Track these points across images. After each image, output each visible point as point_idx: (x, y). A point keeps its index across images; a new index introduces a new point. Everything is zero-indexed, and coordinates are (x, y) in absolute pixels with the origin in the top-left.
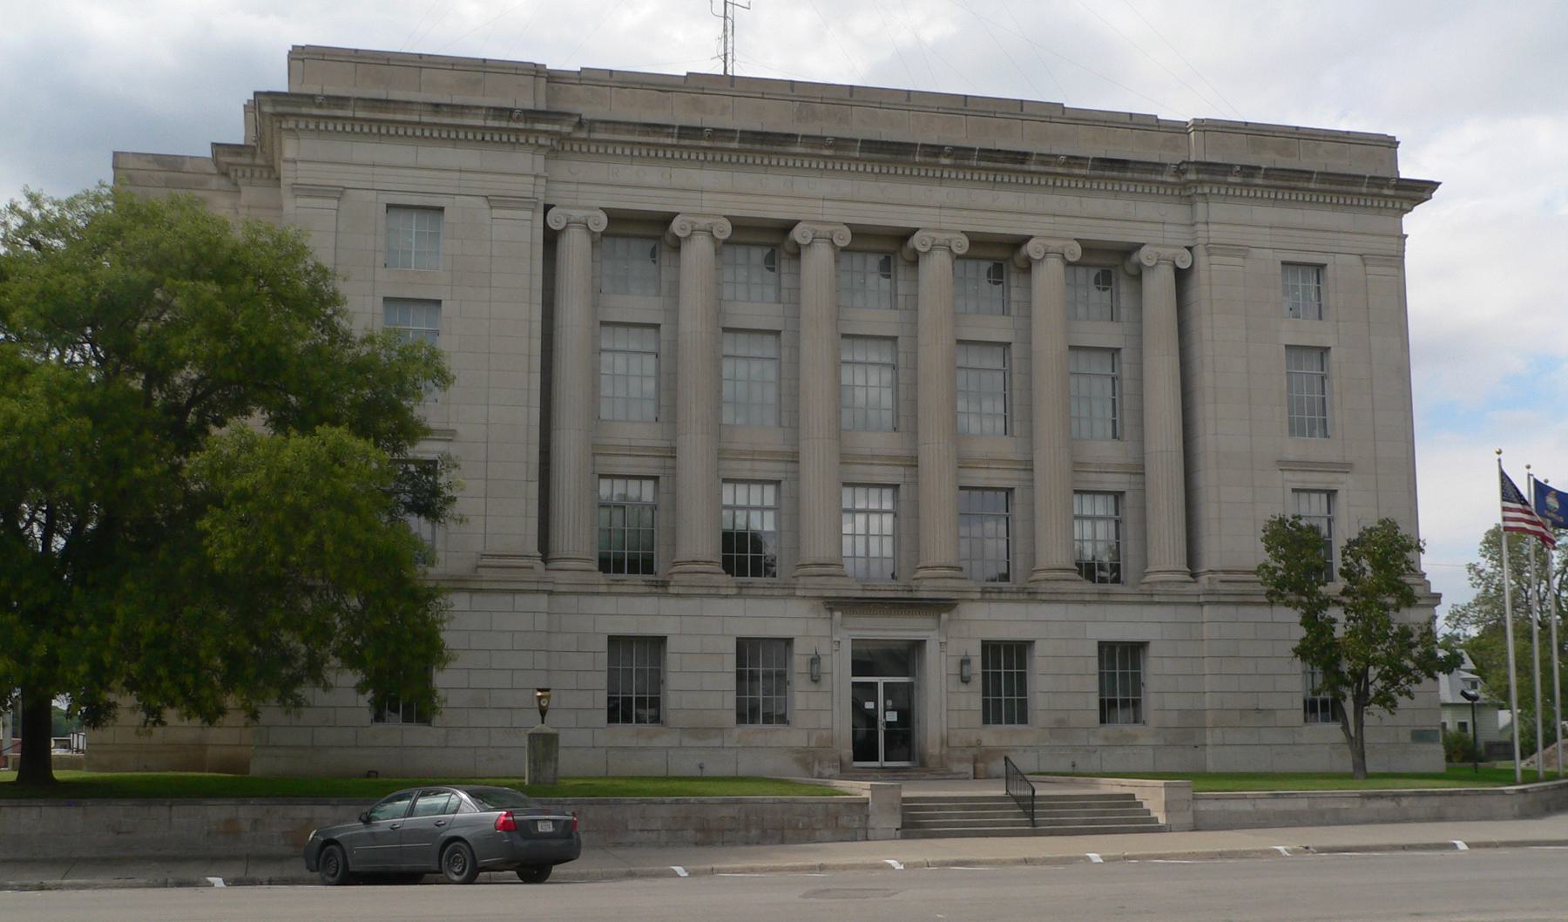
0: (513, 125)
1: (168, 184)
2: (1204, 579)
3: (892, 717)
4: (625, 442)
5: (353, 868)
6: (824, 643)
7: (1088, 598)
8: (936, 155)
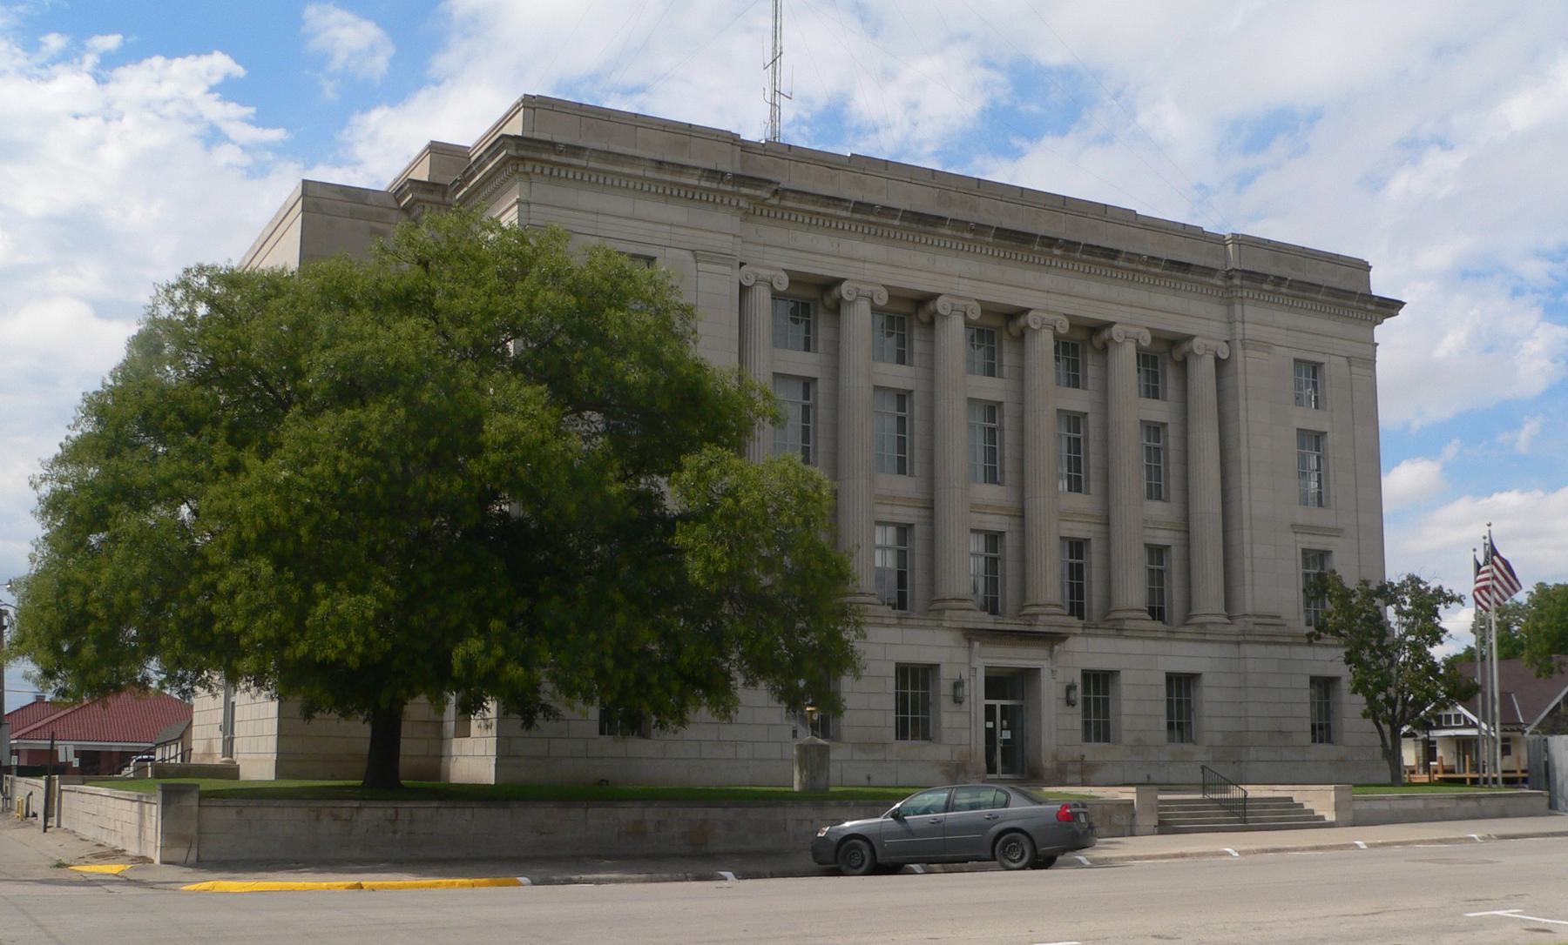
0: (722, 187)
1: (353, 214)
3: (1007, 735)
6: (961, 663)
8: (1050, 246)
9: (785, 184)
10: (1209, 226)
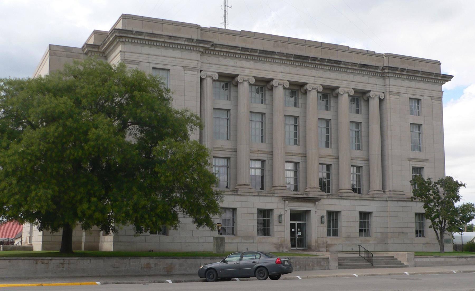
0: (193, 44)
1: (67, 56)
2: (388, 193)
3: (300, 234)
4: (221, 147)
5: (219, 276)
6: (282, 210)
7: (356, 198)
8: (315, 60)
9: (215, 43)
10: (377, 51)
